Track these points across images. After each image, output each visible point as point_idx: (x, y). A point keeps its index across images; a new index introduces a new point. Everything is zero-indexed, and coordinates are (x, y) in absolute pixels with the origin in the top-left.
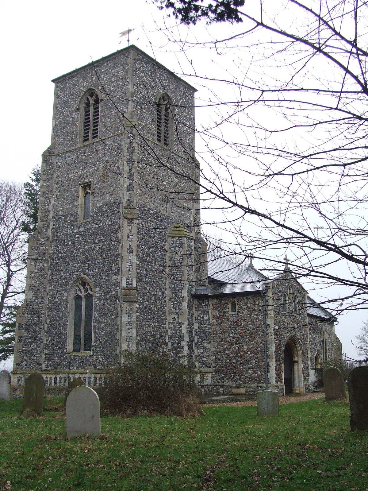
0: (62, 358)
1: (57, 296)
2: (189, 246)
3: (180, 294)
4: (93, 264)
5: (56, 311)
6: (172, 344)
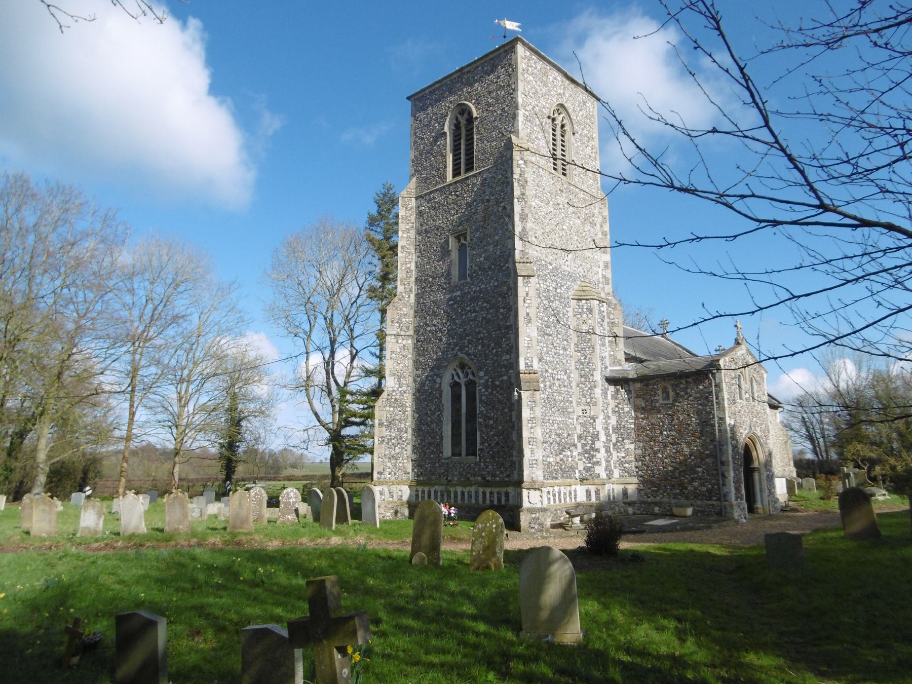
0: (437, 465)
1: (427, 382)
2: (601, 312)
3: (591, 377)
6: (583, 445)
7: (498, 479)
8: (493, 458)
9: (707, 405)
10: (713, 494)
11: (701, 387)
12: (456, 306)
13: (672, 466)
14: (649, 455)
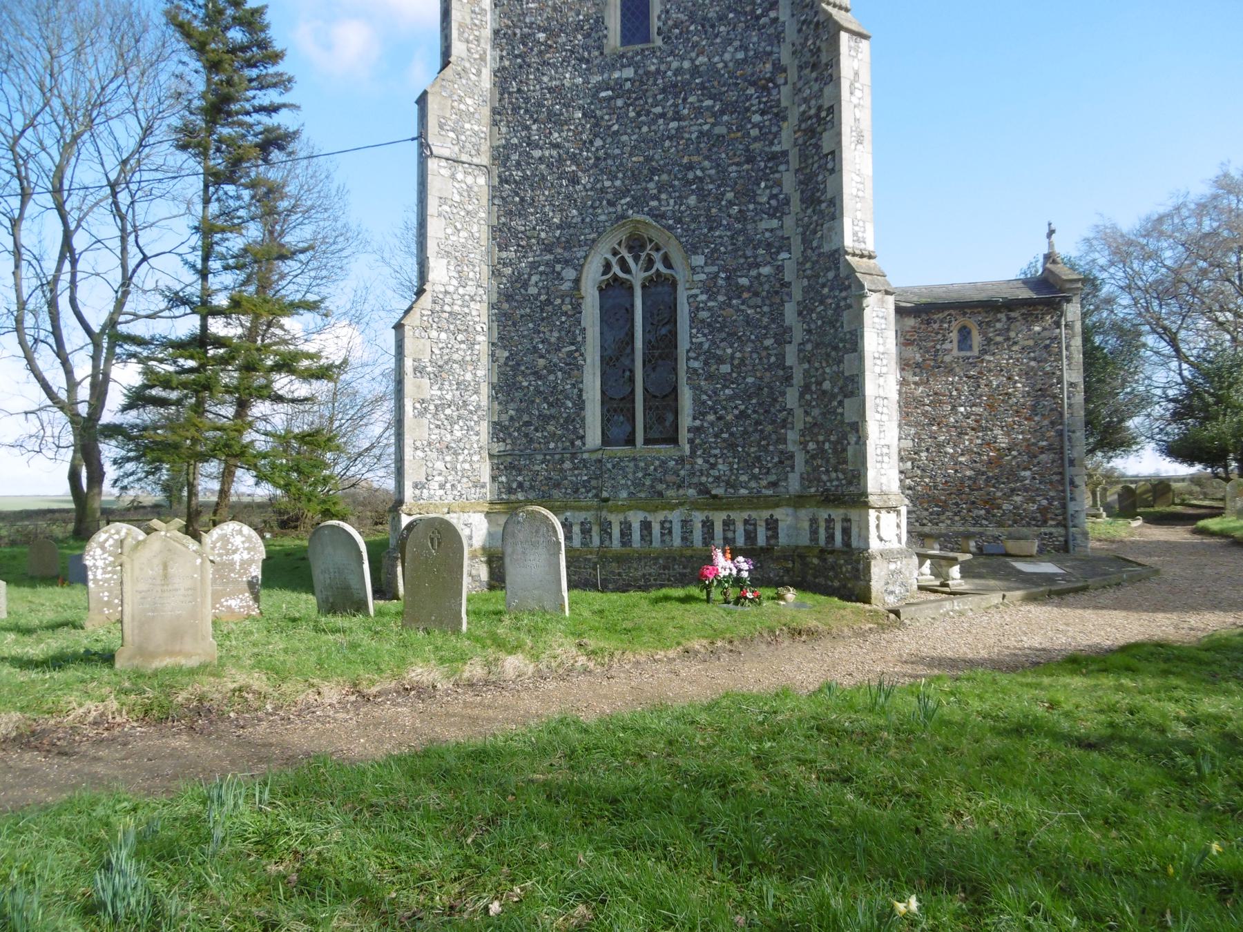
0: (567, 465)
1: (534, 278)
4: (676, 183)
5: (531, 325)
7: (743, 491)
8: (732, 446)
9: (1046, 361)
10: (1049, 516)
11: (1037, 329)
12: (620, 103)
13: (972, 469)
14: (927, 450)
